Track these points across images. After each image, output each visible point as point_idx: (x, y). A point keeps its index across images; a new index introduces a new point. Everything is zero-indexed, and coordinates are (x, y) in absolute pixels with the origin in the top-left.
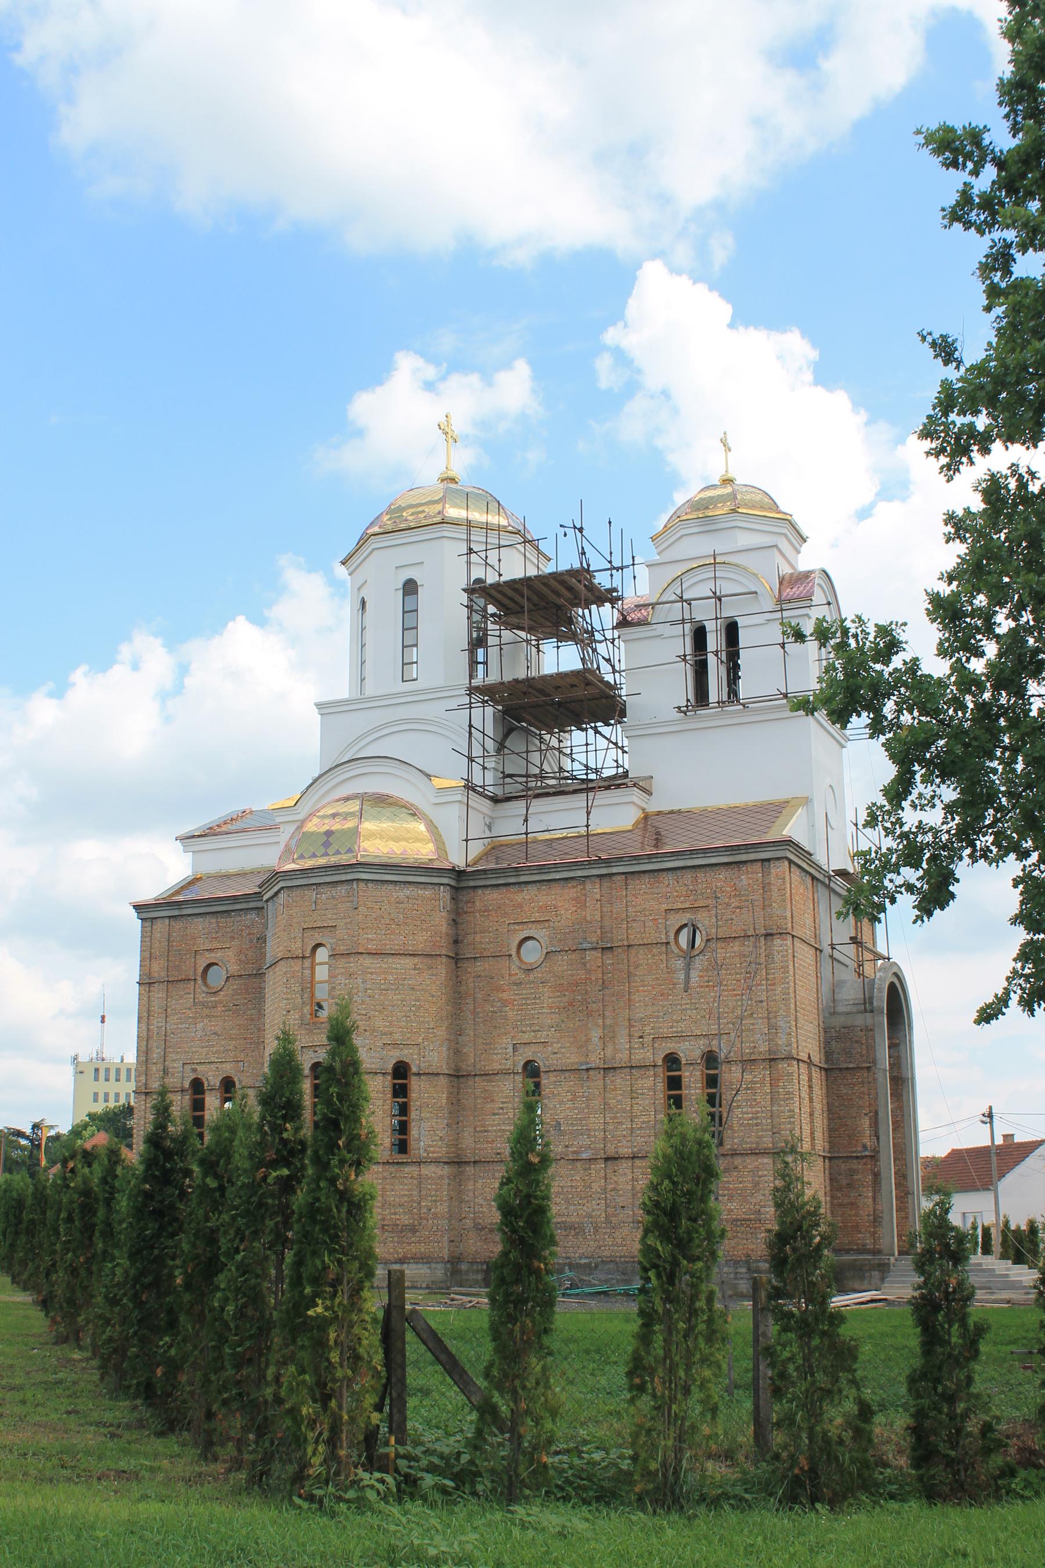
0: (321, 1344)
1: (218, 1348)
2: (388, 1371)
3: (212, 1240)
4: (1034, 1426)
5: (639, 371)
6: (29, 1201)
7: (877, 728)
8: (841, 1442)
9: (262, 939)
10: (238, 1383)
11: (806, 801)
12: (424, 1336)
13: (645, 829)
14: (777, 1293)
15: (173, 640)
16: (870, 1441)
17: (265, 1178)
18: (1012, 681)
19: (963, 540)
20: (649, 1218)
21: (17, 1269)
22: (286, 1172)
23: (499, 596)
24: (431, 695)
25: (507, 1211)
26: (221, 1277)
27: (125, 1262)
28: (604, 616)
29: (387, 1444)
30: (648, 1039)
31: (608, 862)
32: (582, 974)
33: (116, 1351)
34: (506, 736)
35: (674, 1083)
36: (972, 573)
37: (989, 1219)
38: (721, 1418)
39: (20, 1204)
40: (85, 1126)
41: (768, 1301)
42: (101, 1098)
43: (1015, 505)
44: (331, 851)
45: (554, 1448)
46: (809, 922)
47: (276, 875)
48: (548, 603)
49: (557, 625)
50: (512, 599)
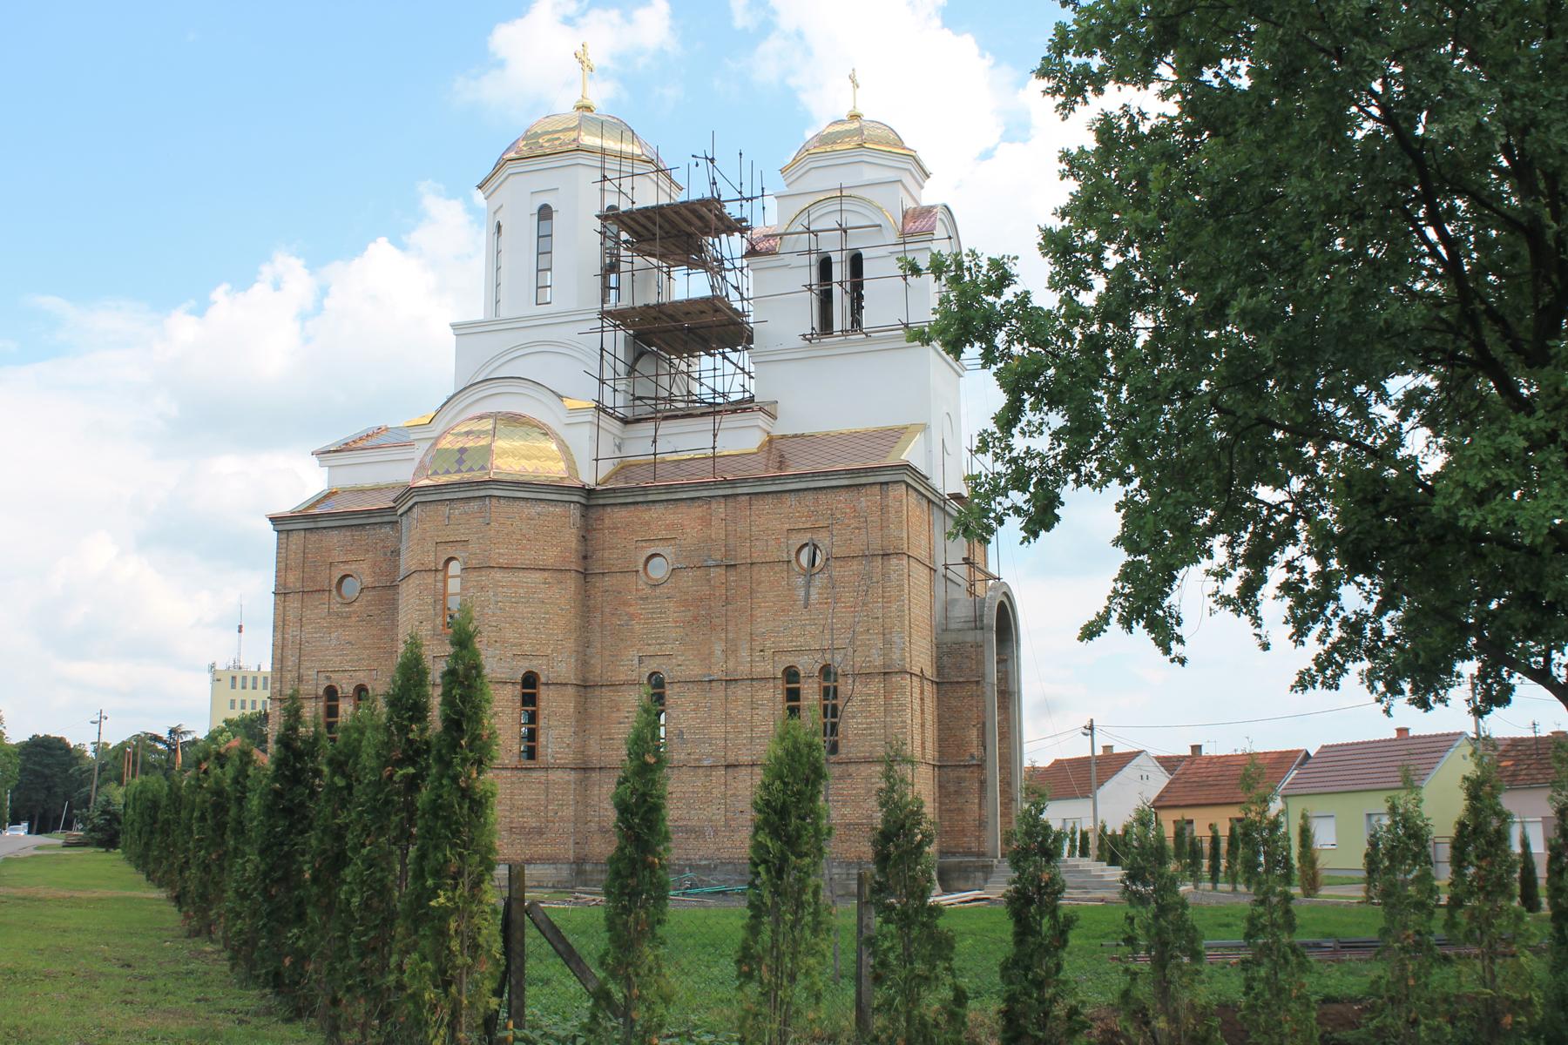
0: (442, 933)
1: (343, 938)
2: (508, 960)
3: (339, 835)
4: (1117, 1010)
5: (774, 12)
6: (164, 802)
7: (988, 358)
8: (937, 1025)
9: (396, 553)
10: (363, 970)
11: (924, 428)
12: (543, 926)
13: (769, 451)
14: (880, 889)
15: (315, 262)
16: (964, 1023)
17: (391, 776)
18: (1119, 314)
19: (1077, 177)
20: (761, 817)
21: (151, 866)
22: (411, 770)
23: (632, 224)
24: (565, 319)
25: (623, 808)
26: (347, 871)
27: (255, 858)
28: (733, 245)
29: (506, 1028)
30: (768, 653)
31: (733, 483)
32: (706, 590)
33: (246, 942)
34: (636, 360)
35: (793, 695)
36: (1084, 209)
37: (1087, 825)
38: (824, 1005)
39: (155, 805)
40: (222, 731)
41: (873, 895)
42: (238, 705)
43: (1126, 144)
44: (463, 468)
45: (665, 1031)
46: (924, 543)
47: (410, 491)
48: (680, 231)
49: (688, 253)
50: (643, 226)
